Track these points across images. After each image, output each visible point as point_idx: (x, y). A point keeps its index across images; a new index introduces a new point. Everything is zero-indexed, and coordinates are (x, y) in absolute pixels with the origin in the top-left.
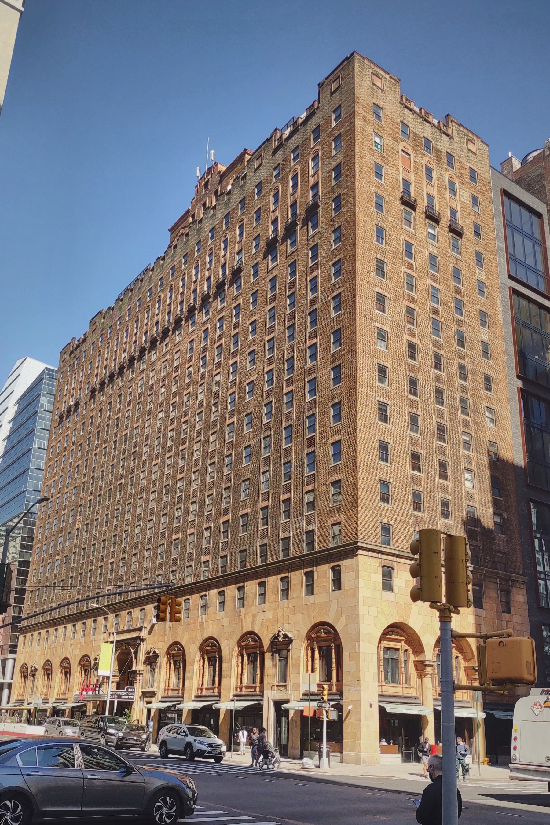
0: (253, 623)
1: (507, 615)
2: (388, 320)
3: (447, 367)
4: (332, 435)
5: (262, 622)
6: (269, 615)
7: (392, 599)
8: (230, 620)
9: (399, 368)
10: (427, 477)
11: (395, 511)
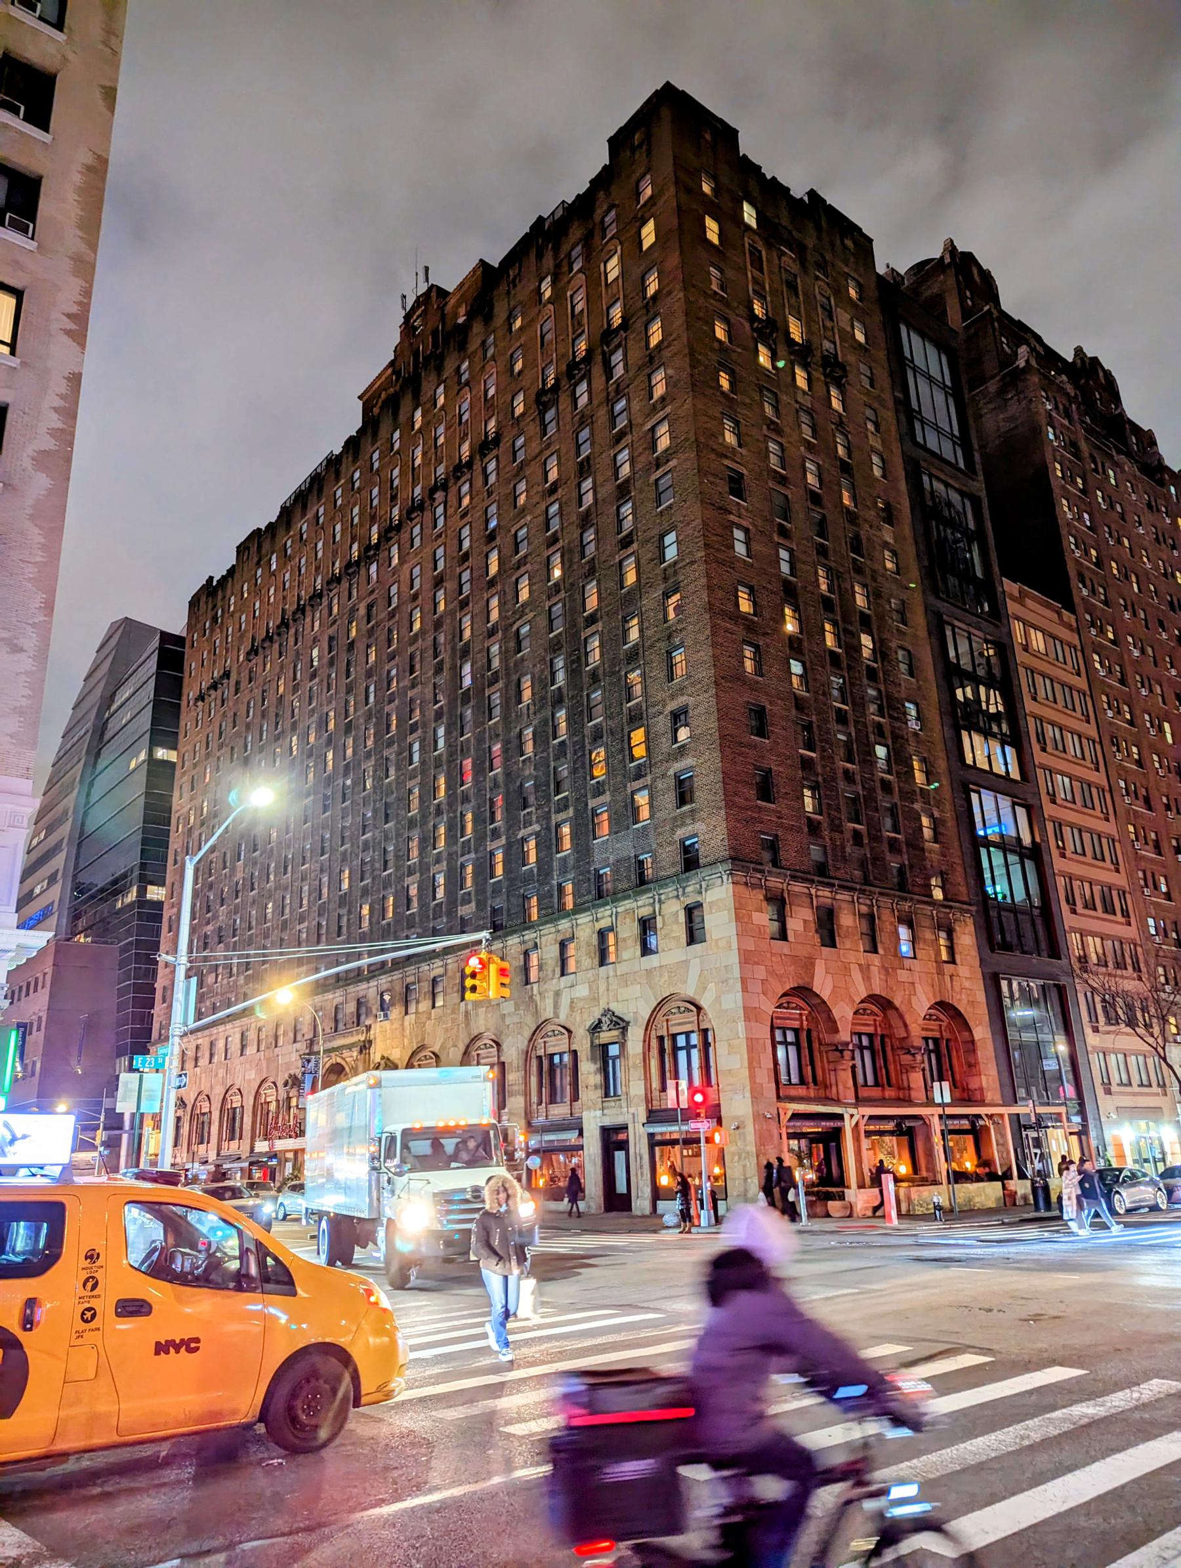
0: (556, 1006)
1: (952, 966)
2: (747, 510)
3: (839, 586)
4: (673, 697)
5: (572, 1002)
6: (582, 991)
7: (786, 951)
8: (516, 1004)
9: (769, 586)
10: (822, 758)
11: (780, 812)
